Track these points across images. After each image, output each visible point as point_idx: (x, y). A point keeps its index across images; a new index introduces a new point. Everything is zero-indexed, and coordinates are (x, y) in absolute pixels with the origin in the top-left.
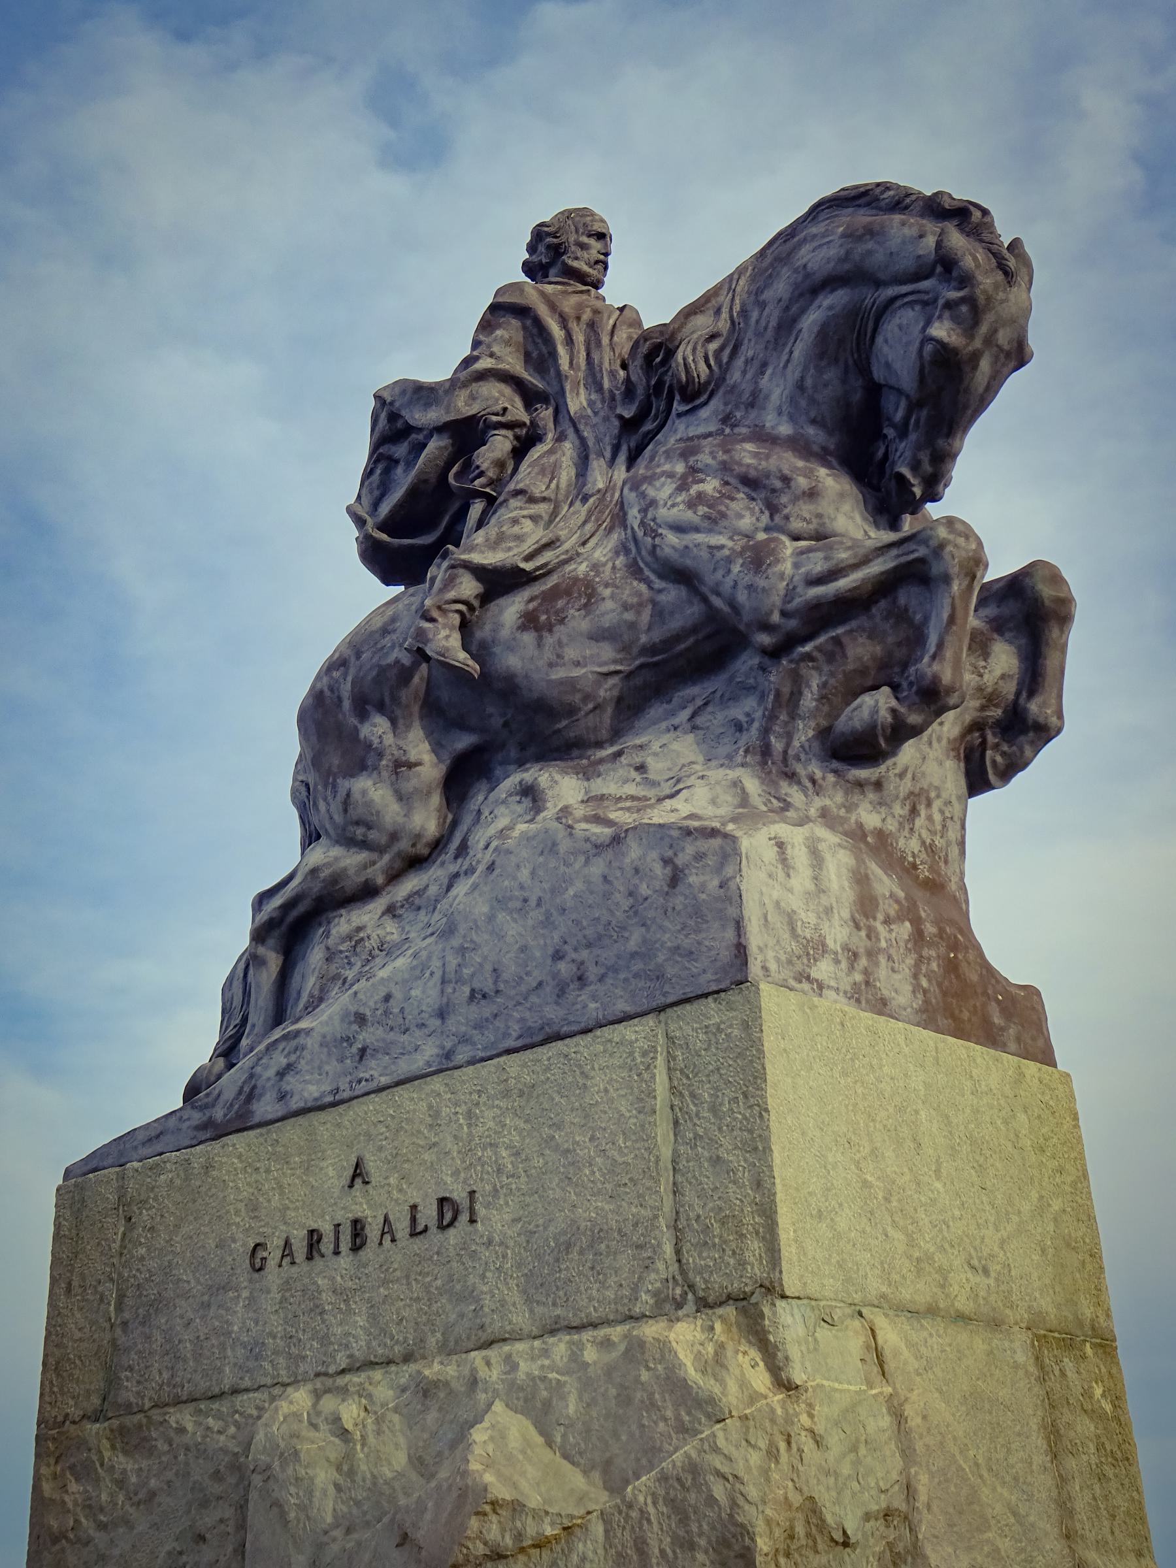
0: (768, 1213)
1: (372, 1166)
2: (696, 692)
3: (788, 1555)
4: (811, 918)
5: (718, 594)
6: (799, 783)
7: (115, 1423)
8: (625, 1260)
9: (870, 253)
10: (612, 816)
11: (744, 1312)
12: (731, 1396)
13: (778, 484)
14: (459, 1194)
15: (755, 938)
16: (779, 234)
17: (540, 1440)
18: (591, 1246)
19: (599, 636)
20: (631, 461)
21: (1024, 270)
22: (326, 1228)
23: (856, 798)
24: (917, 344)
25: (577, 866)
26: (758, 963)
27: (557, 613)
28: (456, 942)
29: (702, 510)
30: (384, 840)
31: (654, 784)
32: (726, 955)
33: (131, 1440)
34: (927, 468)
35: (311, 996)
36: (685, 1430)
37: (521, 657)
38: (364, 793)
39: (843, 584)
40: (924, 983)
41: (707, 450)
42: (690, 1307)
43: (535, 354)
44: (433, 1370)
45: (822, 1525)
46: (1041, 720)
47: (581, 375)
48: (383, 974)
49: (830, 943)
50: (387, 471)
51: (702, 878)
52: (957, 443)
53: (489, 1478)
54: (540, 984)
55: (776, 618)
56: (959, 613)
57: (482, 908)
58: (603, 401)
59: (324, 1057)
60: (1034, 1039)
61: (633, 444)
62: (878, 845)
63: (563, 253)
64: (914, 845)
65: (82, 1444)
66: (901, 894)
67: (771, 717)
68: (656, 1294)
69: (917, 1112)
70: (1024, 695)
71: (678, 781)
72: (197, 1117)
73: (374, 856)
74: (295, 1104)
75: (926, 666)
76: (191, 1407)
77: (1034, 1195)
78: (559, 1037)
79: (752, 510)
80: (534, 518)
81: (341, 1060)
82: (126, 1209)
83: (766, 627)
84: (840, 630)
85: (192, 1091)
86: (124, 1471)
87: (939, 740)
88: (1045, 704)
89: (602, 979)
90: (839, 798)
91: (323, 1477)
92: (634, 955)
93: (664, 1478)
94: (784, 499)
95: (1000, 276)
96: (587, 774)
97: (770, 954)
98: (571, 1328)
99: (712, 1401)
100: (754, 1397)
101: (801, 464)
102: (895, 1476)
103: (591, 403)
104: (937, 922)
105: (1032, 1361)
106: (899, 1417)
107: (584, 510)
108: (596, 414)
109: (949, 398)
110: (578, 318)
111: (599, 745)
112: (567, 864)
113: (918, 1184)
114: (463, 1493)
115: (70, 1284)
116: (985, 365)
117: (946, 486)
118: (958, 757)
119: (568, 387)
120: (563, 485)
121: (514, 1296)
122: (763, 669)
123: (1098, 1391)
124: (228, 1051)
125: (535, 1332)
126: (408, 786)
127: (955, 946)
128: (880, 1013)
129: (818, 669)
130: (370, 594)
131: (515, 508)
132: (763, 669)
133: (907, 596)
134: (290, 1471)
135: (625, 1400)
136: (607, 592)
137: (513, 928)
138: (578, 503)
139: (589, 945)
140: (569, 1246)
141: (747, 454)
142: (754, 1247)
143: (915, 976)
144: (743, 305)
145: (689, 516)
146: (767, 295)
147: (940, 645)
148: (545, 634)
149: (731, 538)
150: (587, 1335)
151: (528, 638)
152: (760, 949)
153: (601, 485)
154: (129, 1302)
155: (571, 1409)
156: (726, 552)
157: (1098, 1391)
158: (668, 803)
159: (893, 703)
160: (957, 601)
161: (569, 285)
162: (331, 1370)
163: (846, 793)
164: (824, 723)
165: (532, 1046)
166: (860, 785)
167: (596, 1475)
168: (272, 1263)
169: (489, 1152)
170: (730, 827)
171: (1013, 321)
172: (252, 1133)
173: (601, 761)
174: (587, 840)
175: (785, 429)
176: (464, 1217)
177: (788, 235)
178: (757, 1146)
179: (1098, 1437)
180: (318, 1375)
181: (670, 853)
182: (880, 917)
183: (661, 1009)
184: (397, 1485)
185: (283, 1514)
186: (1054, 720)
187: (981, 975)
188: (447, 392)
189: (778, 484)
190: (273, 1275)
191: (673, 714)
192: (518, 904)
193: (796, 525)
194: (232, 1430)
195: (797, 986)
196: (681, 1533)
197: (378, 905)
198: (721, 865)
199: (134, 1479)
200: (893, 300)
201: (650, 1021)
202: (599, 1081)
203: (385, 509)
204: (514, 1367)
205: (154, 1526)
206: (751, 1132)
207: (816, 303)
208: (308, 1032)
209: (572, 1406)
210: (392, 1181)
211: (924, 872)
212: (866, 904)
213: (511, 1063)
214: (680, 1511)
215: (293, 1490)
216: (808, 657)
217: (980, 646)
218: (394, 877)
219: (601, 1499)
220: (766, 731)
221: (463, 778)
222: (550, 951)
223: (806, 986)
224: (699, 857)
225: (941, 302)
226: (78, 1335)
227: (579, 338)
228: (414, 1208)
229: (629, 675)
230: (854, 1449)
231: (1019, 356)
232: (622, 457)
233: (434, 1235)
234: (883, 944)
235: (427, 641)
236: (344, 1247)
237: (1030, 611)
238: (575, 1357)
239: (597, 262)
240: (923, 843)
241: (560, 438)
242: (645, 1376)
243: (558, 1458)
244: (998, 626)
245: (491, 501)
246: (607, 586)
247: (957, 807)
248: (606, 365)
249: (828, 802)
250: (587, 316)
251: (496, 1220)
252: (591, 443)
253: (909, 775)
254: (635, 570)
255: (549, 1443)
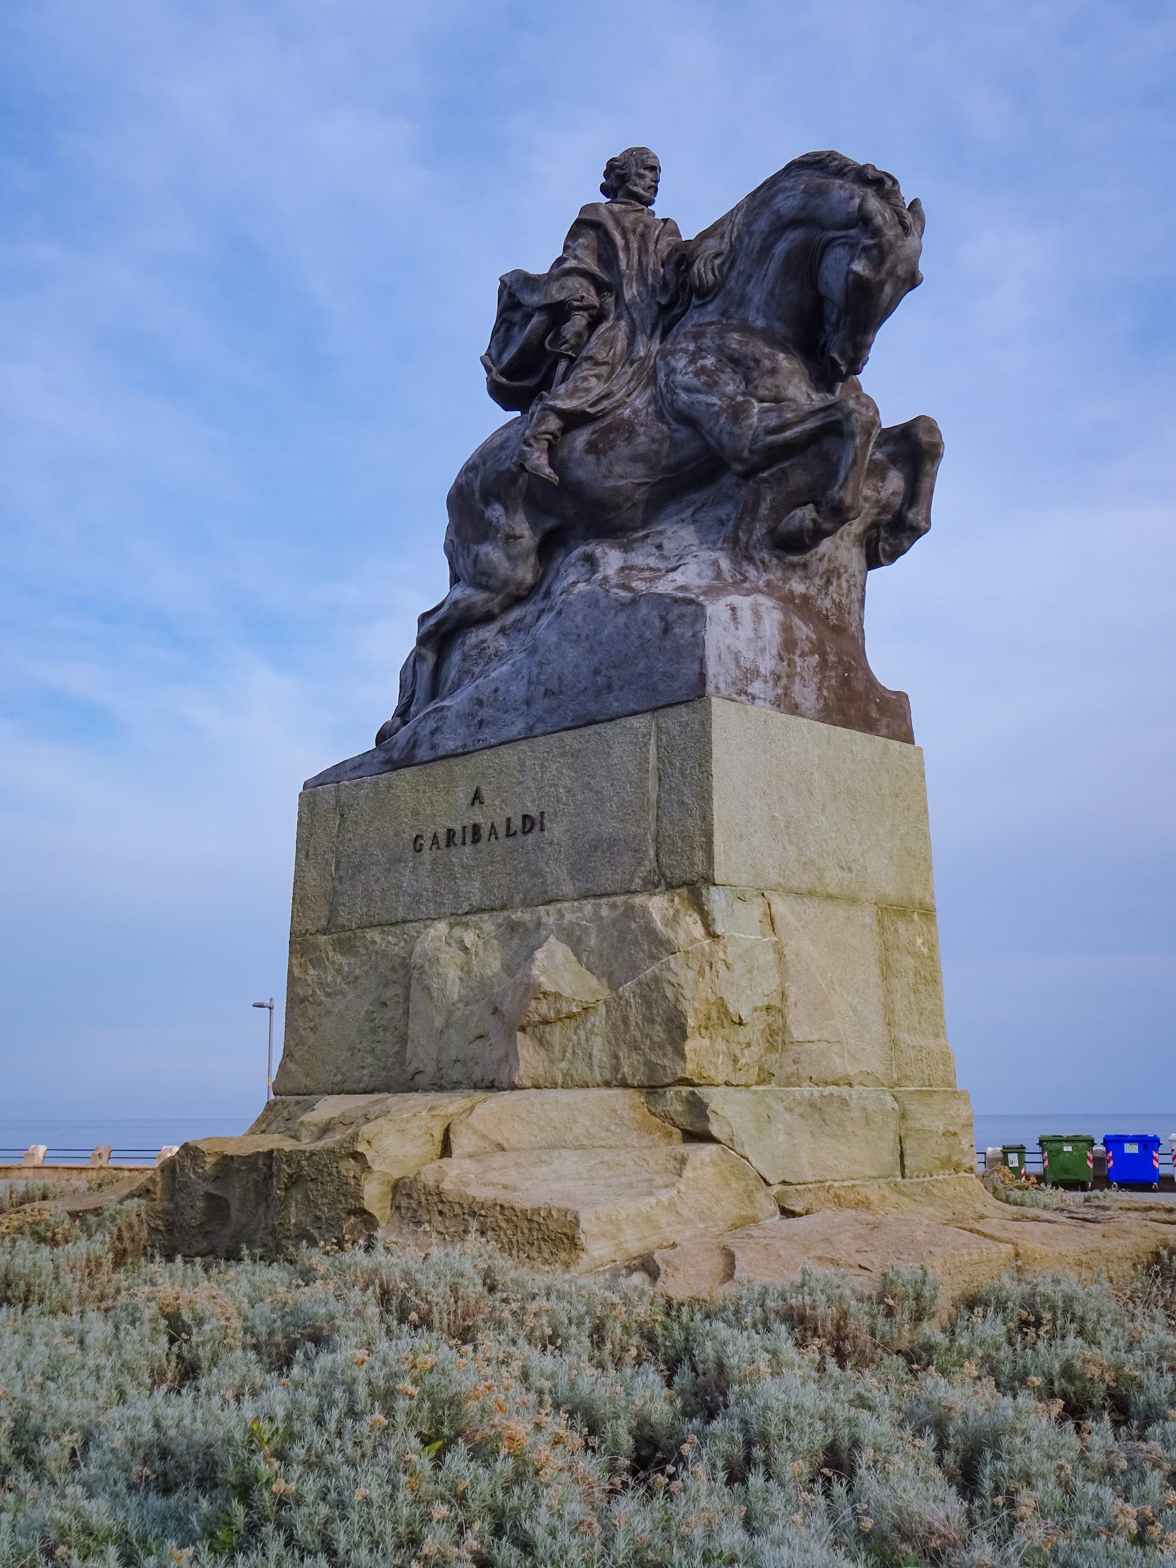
0: (709, 835)
1: (485, 792)
2: (697, 497)
3: (706, 1028)
4: (751, 655)
5: (711, 436)
6: (754, 564)
7: (336, 936)
8: (627, 858)
9: (818, 206)
10: (634, 584)
11: (691, 892)
12: (680, 939)
13: (752, 364)
14: (534, 812)
15: (712, 668)
16: (765, 182)
17: (574, 959)
18: (609, 848)
19: (635, 459)
20: (663, 338)
21: (918, 223)
22: (458, 828)
23: (790, 574)
24: (844, 274)
25: (610, 616)
26: (713, 685)
27: (610, 442)
28: (537, 659)
29: (703, 378)
30: (499, 585)
31: (666, 558)
32: (694, 679)
33: (345, 946)
34: (851, 354)
35: (453, 683)
36: (654, 958)
37: (586, 471)
38: (487, 554)
39: (788, 434)
40: (825, 693)
41: (709, 336)
42: (662, 888)
43: (604, 256)
44: (518, 915)
45: (727, 1013)
46: (915, 524)
47: (634, 272)
48: (494, 675)
49: (762, 670)
50: (508, 331)
51: (682, 630)
52: (870, 338)
53: (542, 979)
54: (586, 689)
55: (746, 454)
56: (859, 458)
57: (553, 639)
58: (647, 292)
59: (458, 724)
60: (900, 726)
61: (666, 323)
62: (802, 606)
63: (629, 178)
64: (828, 603)
65: (316, 947)
66: (814, 637)
67: (740, 519)
68: (644, 879)
69: (812, 774)
70: (906, 506)
71: (681, 558)
72: (382, 756)
73: (493, 595)
74: (441, 752)
75: (836, 493)
76: (378, 929)
77: (888, 824)
78: (594, 722)
79: (734, 380)
80: (598, 377)
81: (468, 727)
82: (341, 809)
83: (740, 460)
84: (786, 464)
85: (381, 737)
86: (341, 964)
87: (848, 535)
88: (917, 514)
89: (622, 688)
90: (779, 574)
91: (453, 973)
92: (640, 675)
93: (640, 983)
94: (755, 374)
95: (900, 230)
96: (626, 548)
97: (721, 679)
98: (596, 896)
99: (669, 942)
100: (693, 941)
101: (767, 350)
102: (774, 987)
103: (640, 293)
104: (837, 654)
105: (876, 923)
106: (780, 954)
107: (630, 371)
108: (642, 301)
109: (866, 309)
110: (634, 231)
111: (635, 530)
112: (604, 614)
113: (809, 818)
114: (528, 987)
115: (308, 853)
116: (888, 289)
117: (864, 364)
118: (861, 546)
119: (625, 282)
120: (618, 351)
121: (564, 875)
122: (738, 486)
123: (919, 942)
124: (403, 713)
125: (576, 896)
126: (514, 552)
127: (849, 668)
128: (793, 714)
129: (771, 489)
130: (498, 417)
131: (585, 370)
132: (738, 486)
133: (828, 444)
134: (434, 969)
135: (622, 939)
136: (642, 430)
137: (572, 653)
138: (627, 366)
139: (614, 667)
140: (596, 847)
141: (734, 340)
142: (700, 855)
143: (819, 689)
144: (739, 234)
145: (695, 382)
146: (754, 227)
147: (846, 480)
148: (602, 456)
149: (720, 399)
150: (603, 901)
151: (591, 458)
152: (715, 676)
153: (642, 354)
154: (343, 865)
155: (592, 942)
156: (717, 408)
157: (919, 942)
158: (671, 576)
159: (814, 515)
160: (859, 452)
161: (630, 204)
162: (460, 912)
163: (784, 571)
164: (772, 525)
165: (580, 727)
166: (793, 566)
167: (604, 980)
168: (426, 847)
169: (553, 789)
170: (702, 598)
171: (908, 259)
172: (415, 768)
173: (635, 540)
174: (617, 600)
175: (760, 323)
176: (538, 827)
177: (771, 184)
178: (705, 796)
179: (916, 968)
180: (452, 914)
181: (664, 613)
182: (798, 652)
183: (654, 710)
184: (494, 980)
185: (430, 994)
186: (923, 524)
187: (866, 687)
188: (545, 283)
189: (752, 364)
190: (427, 855)
191: (681, 511)
192: (574, 638)
193: (762, 392)
194: (403, 943)
195: (738, 698)
196: (648, 1014)
197: (495, 627)
198: (692, 625)
199: (346, 969)
200: (833, 239)
201: (648, 716)
202: (617, 750)
203: (506, 358)
204: (562, 916)
205: (358, 996)
206: (701, 787)
207: (785, 236)
208: (449, 708)
209: (593, 941)
210: (497, 803)
211: (833, 620)
212: (789, 644)
213: (568, 736)
214: (647, 1002)
215: (435, 980)
216: (766, 480)
217: (878, 471)
218: (506, 608)
219: (606, 993)
220: (737, 528)
221: (550, 547)
222: (592, 668)
223: (743, 698)
224: (682, 616)
225: (860, 246)
226: (313, 883)
227: (634, 245)
228: (509, 820)
229: (655, 484)
230: (750, 971)
231: (912, 280)
232: (658, 333)
233: (521, 838)
234: (799, 670)
235: (526, 460)
236: (468, 841)
237: (914, 449)
238: (596, 913)
239: (650, 187)
240: (834, 602)
241: (618, 318)
242: (633, 926)
243: (584, 970)
244: (893, 459)
245: (572, 360)
246: (642, 425)
247: (859, 578)
248: (651, 266)
249: (771, 577)
250: (640, 229)
251: (556, 830)
252: (637, 323)
253: (826, 559)
254: (660, 416)
255: (580, 961)
